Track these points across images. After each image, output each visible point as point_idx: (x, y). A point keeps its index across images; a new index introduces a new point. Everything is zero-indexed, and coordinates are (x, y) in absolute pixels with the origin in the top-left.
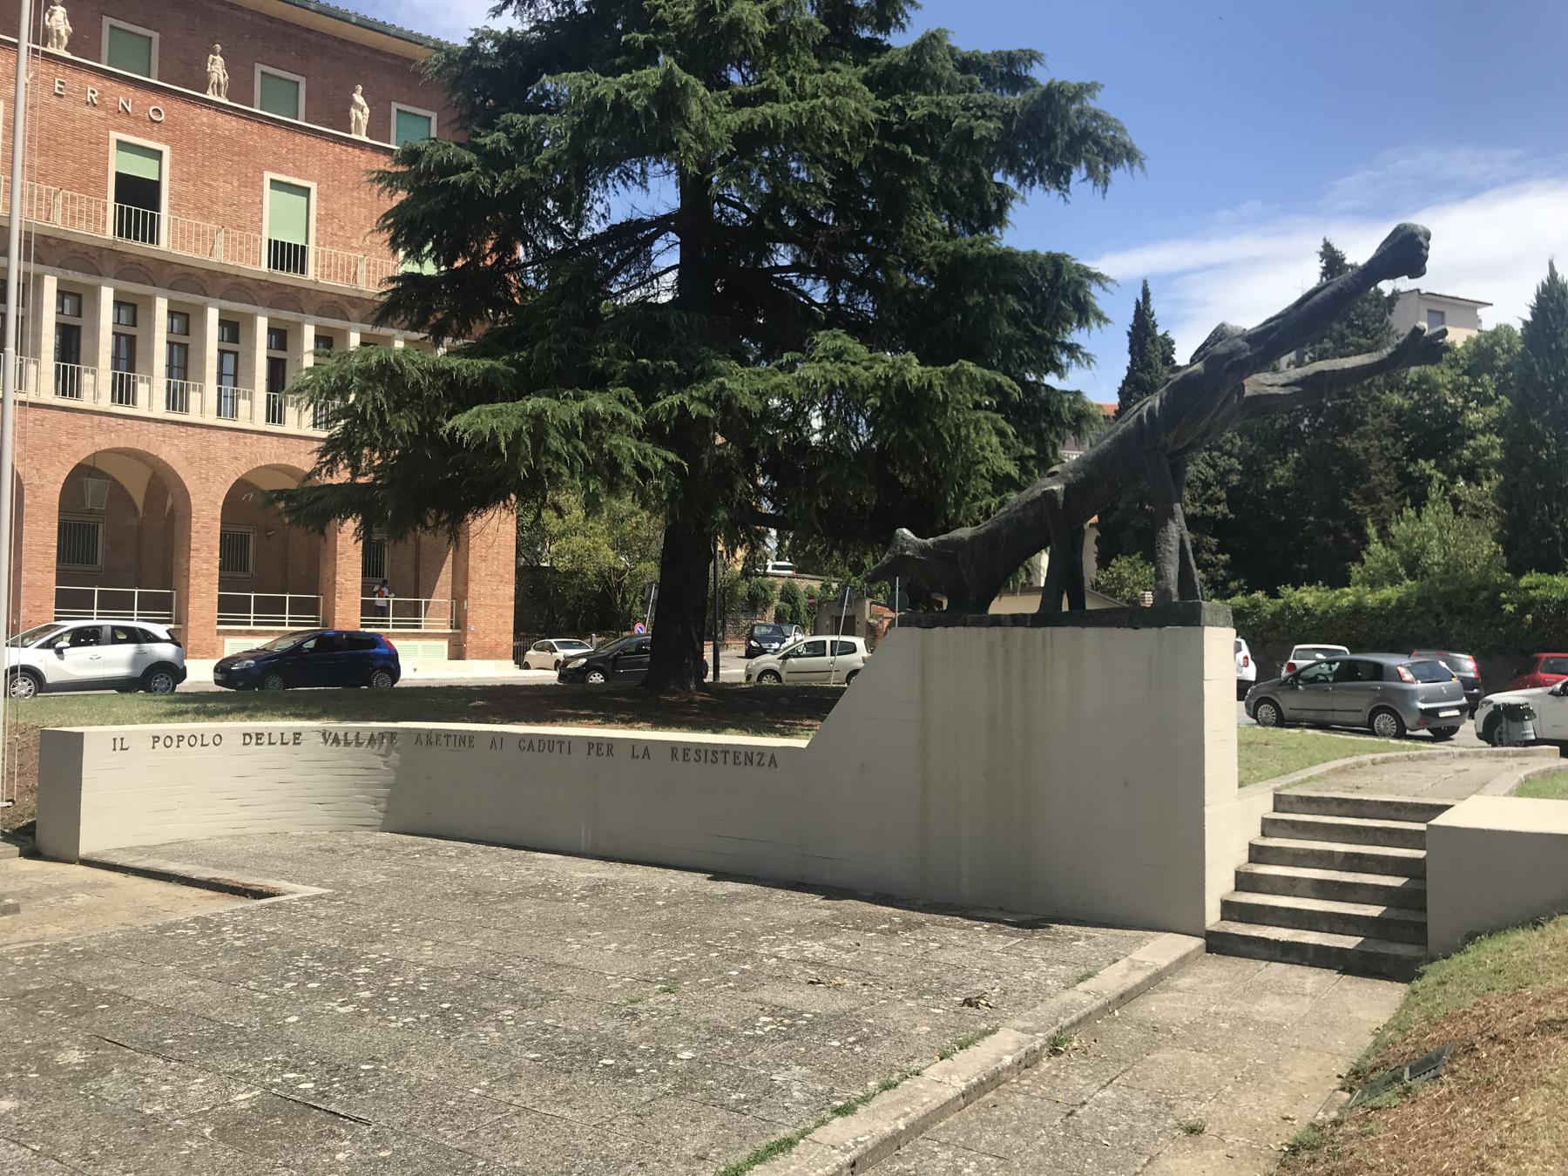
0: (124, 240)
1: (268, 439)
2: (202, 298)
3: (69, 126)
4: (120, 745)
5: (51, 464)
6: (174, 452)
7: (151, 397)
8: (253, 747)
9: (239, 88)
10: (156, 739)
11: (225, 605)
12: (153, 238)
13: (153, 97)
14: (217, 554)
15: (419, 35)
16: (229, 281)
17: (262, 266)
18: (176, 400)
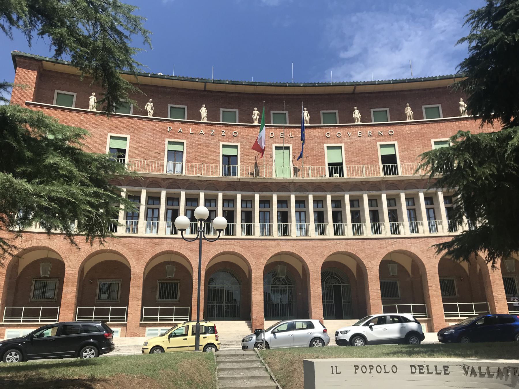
0: (386, 176)
2: (417, 190)
3: (364, 145)
4: (335, 370)
5: (374, 259)
6: (416, 249)
7: (405, 230)
8: (417, 375)
9: (417, 114)
10: (356, 367)
11: (447, 309)
12: (396, 173)
14: (439, 287)
16: (425, 181)
18: (414, 229)
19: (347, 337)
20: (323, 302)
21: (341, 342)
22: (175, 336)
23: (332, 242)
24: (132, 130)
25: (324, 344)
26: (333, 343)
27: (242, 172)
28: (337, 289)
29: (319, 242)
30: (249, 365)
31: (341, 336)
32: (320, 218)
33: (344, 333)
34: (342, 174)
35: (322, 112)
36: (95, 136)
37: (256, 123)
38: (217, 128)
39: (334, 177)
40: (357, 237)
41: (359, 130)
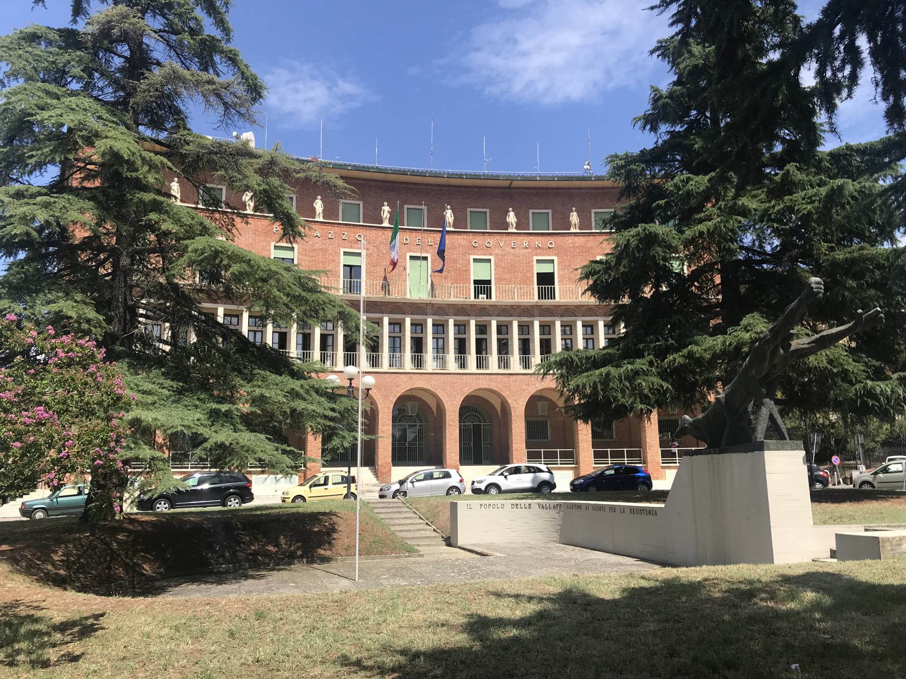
3: (518, 259)
4: (469, 507)
10: (481, 505)
13: (549, 238)
19: (482, 486)
20: (460, 444)
21: (476, 491)
22: (316, 485)
23: (474, 377)
25: (460, 493)
26: (469, 492)
27: (367, 290)
28: (477, 429)
29: (459, 376)
30: (399, 510)
31: (477, 486)
32: (462, 347)
33: (480, 482)
34: (489, 296)
35: (469, 210)
37: (386, 224)
38: (337, 229)
39: (480, 299)
40: (502, 371)
41: (513, 239)
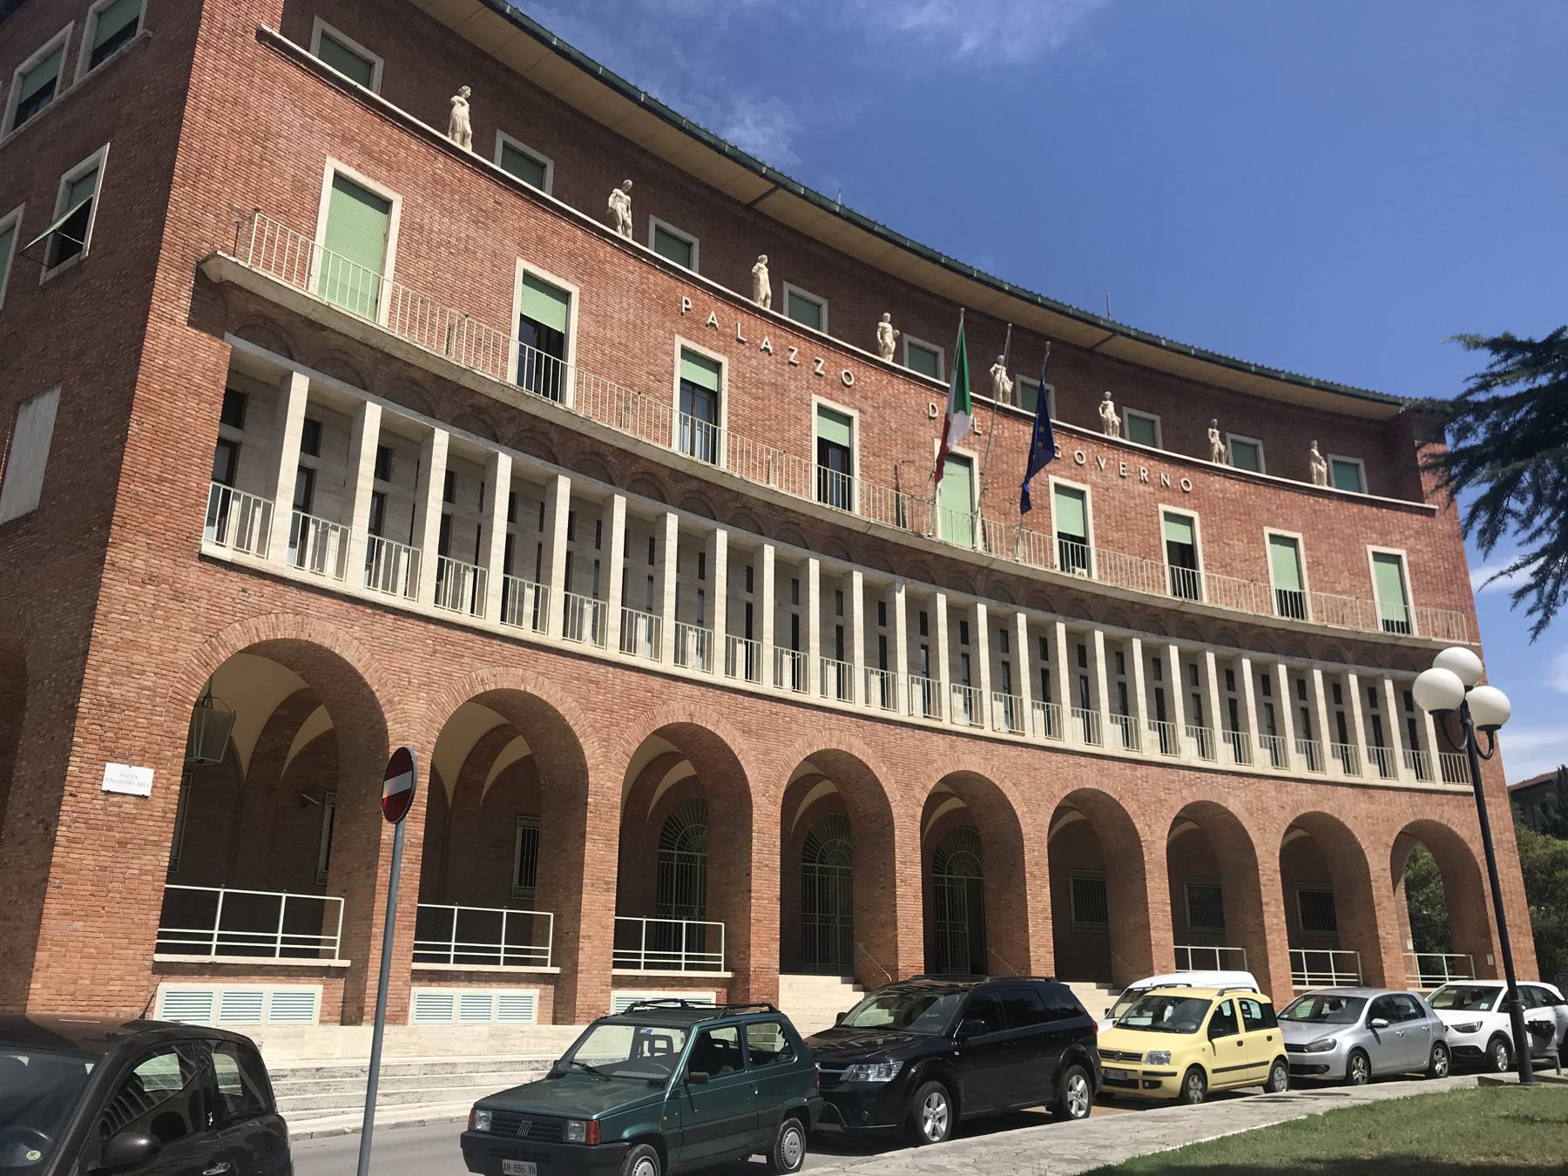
1: (1303, 786)
2: (1237, 650)
11: (625, 936)
15: (1213, 354)
17: (1274, 613)
23: (1071, 759)
24: (586, 271)
27: (865, 507)
29: (1043, 754)
36: (479, 255)
